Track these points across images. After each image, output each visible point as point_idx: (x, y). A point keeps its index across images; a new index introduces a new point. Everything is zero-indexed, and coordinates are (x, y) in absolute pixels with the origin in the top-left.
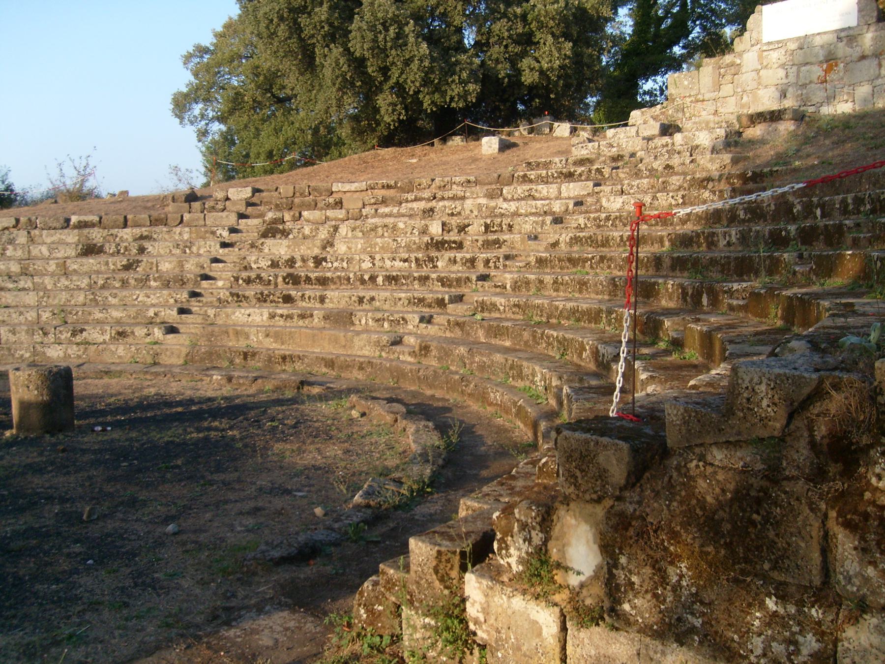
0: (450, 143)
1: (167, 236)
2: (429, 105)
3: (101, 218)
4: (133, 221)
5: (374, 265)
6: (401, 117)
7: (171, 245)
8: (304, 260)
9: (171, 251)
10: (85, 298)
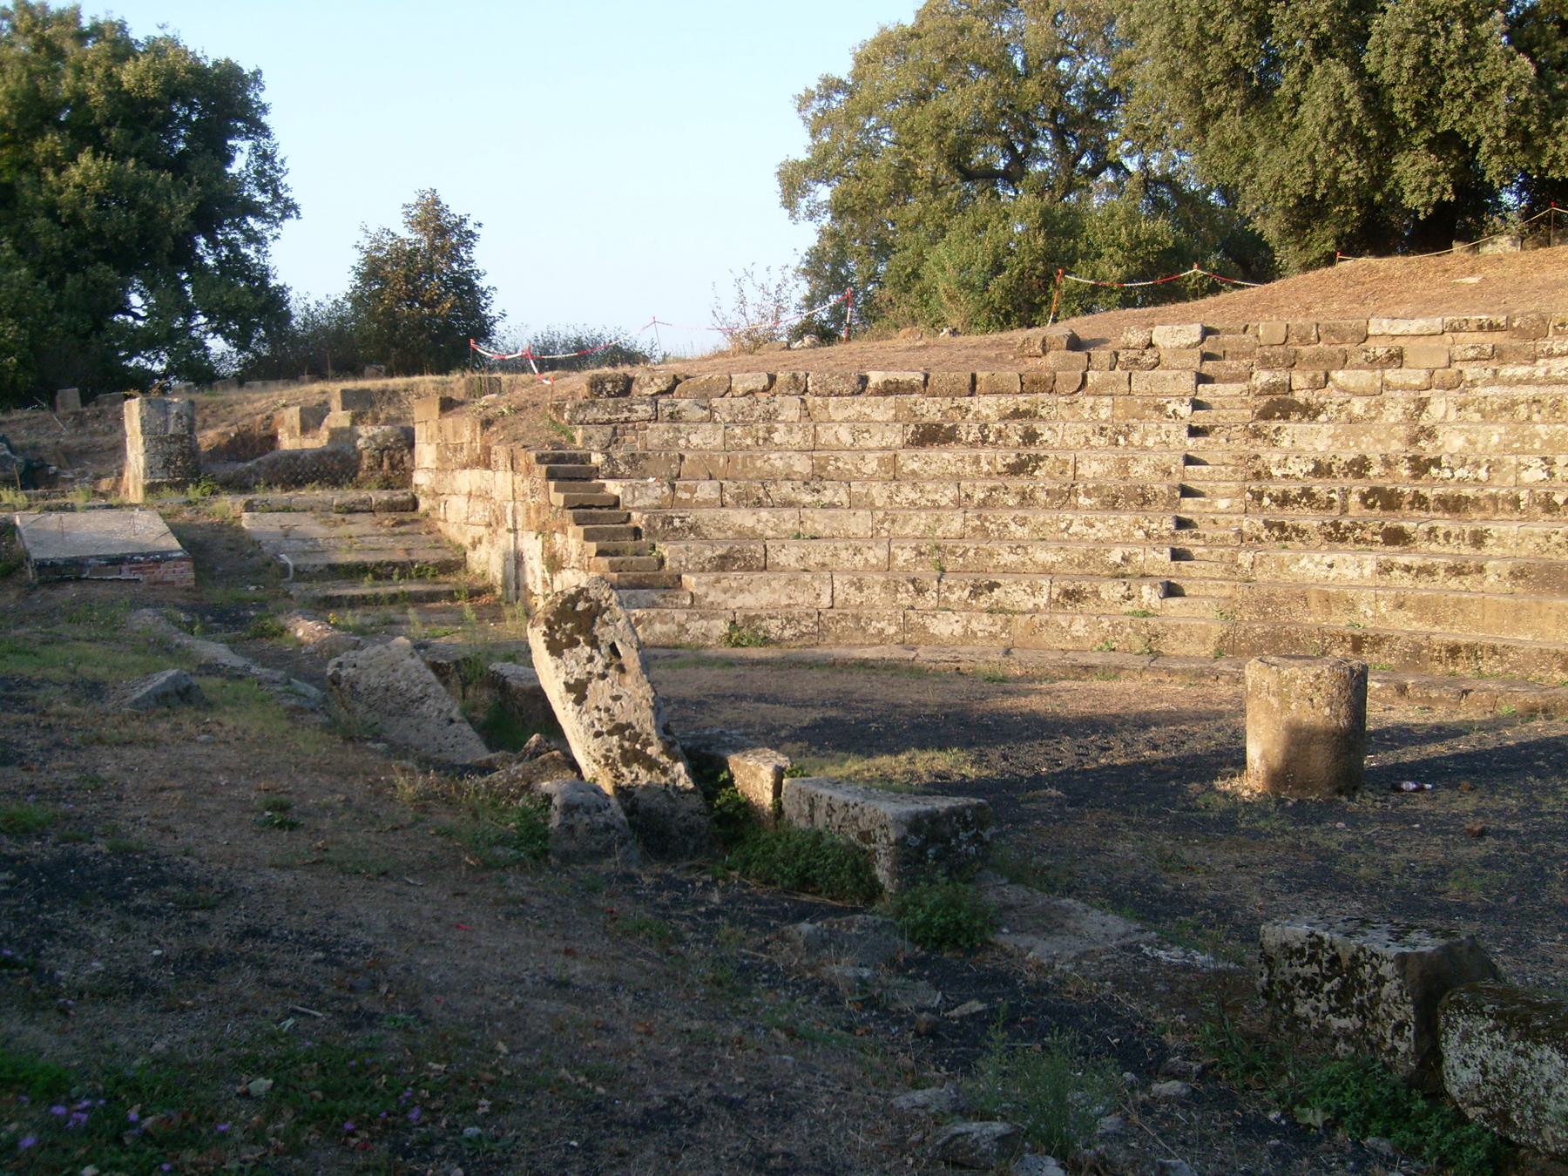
0: (1487, 250)
1: (1066, 413)
2: (1498, 174)
3: (927, 377)
4: (988, 382)
5: (1551, 475)
6: (1446, 198)
7: (1089, 428)
8: (1387, 463)
9: (1087, 440)
10: (965, 525)
